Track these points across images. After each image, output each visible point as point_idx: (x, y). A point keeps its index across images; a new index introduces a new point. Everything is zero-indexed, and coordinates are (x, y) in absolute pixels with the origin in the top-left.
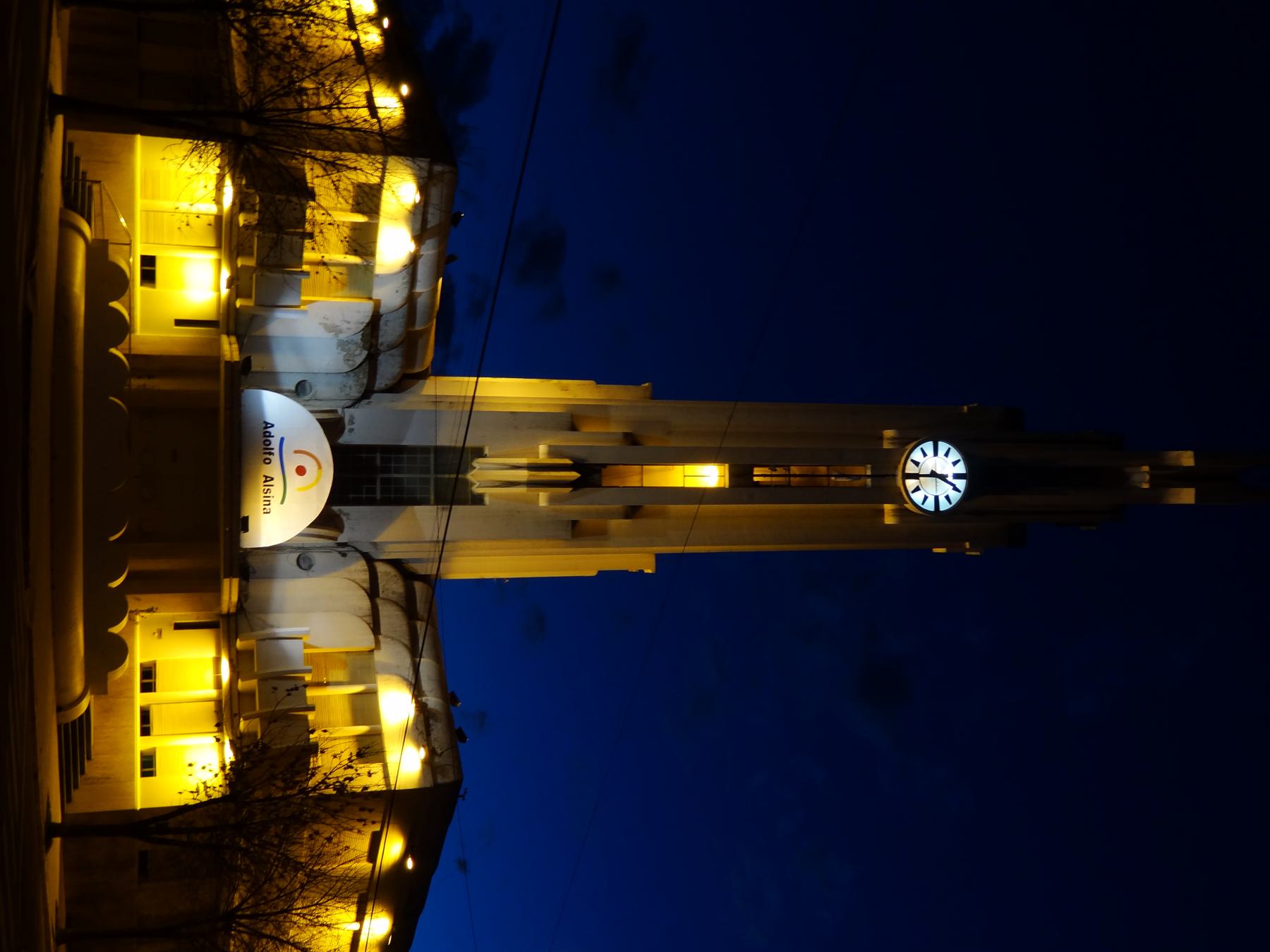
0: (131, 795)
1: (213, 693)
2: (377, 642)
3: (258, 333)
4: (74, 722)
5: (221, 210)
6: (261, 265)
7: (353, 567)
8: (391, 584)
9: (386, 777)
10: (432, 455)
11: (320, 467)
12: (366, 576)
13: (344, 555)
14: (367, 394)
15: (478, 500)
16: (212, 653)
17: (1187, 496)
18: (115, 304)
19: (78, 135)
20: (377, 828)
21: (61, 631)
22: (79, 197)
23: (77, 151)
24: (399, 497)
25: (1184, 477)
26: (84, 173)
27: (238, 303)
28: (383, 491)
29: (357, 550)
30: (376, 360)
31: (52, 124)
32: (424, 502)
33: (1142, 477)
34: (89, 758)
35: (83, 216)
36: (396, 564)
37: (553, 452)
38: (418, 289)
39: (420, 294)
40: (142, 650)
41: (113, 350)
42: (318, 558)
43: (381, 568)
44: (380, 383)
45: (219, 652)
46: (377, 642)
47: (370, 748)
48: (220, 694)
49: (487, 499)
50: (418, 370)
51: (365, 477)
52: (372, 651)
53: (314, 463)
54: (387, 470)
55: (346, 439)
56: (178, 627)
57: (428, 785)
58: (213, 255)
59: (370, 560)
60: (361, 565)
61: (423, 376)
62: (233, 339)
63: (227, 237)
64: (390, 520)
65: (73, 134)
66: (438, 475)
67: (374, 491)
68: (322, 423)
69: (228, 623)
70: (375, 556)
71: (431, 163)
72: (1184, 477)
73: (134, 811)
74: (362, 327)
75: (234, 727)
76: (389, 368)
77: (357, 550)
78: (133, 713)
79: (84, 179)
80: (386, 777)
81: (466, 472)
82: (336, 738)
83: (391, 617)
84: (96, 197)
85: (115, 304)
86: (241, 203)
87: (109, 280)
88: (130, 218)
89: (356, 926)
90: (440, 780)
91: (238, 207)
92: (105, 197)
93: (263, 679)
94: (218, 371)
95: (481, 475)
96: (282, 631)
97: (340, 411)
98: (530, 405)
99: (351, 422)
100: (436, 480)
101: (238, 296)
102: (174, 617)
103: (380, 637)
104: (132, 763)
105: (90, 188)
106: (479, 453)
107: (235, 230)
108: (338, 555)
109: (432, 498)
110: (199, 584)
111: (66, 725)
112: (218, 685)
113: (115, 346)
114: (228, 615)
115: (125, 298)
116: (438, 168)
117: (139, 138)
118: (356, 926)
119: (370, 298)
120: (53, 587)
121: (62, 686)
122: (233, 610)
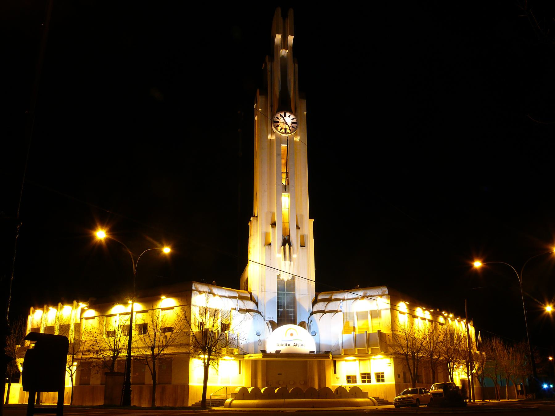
0: (391, 385)
1: (357, 362)
2: (341, 311)
7: (316, 318)
8: (320, 306)
9: (386, 309)
13: (311, 321)
17: (291, 38)
21: (357, 404)
22: (220, 402)
24: (293, 303)
25: (284, 38)
27: (236, 353)
32: (294, 295)
33: (284, 52)
37: (279, 252)
40: (343, 383)
43: (315, 309)
46: (341, 311)
47: (375, 314)
50: (250, 296)
51: (286, 315)
54: (284, 307)
56: (335, 372)
59: (312, 313)
64: (300, 305)
66: (286, 290)
67: (291, 311)
71: (435, 315)
72: (284, 38)
75: (369, 356)
76: (251, 305)
80: (386, 309)
81: (284, 281)
83: (332, 306)
89: (419, 318)
90: (387, 293)
94: (267, 361)
95: (286, 278)
96: (340, 342)
104: (380, 385)
112: (355, 360)
116: (194, 288)
118: (427, 320)
121: (367, 404)
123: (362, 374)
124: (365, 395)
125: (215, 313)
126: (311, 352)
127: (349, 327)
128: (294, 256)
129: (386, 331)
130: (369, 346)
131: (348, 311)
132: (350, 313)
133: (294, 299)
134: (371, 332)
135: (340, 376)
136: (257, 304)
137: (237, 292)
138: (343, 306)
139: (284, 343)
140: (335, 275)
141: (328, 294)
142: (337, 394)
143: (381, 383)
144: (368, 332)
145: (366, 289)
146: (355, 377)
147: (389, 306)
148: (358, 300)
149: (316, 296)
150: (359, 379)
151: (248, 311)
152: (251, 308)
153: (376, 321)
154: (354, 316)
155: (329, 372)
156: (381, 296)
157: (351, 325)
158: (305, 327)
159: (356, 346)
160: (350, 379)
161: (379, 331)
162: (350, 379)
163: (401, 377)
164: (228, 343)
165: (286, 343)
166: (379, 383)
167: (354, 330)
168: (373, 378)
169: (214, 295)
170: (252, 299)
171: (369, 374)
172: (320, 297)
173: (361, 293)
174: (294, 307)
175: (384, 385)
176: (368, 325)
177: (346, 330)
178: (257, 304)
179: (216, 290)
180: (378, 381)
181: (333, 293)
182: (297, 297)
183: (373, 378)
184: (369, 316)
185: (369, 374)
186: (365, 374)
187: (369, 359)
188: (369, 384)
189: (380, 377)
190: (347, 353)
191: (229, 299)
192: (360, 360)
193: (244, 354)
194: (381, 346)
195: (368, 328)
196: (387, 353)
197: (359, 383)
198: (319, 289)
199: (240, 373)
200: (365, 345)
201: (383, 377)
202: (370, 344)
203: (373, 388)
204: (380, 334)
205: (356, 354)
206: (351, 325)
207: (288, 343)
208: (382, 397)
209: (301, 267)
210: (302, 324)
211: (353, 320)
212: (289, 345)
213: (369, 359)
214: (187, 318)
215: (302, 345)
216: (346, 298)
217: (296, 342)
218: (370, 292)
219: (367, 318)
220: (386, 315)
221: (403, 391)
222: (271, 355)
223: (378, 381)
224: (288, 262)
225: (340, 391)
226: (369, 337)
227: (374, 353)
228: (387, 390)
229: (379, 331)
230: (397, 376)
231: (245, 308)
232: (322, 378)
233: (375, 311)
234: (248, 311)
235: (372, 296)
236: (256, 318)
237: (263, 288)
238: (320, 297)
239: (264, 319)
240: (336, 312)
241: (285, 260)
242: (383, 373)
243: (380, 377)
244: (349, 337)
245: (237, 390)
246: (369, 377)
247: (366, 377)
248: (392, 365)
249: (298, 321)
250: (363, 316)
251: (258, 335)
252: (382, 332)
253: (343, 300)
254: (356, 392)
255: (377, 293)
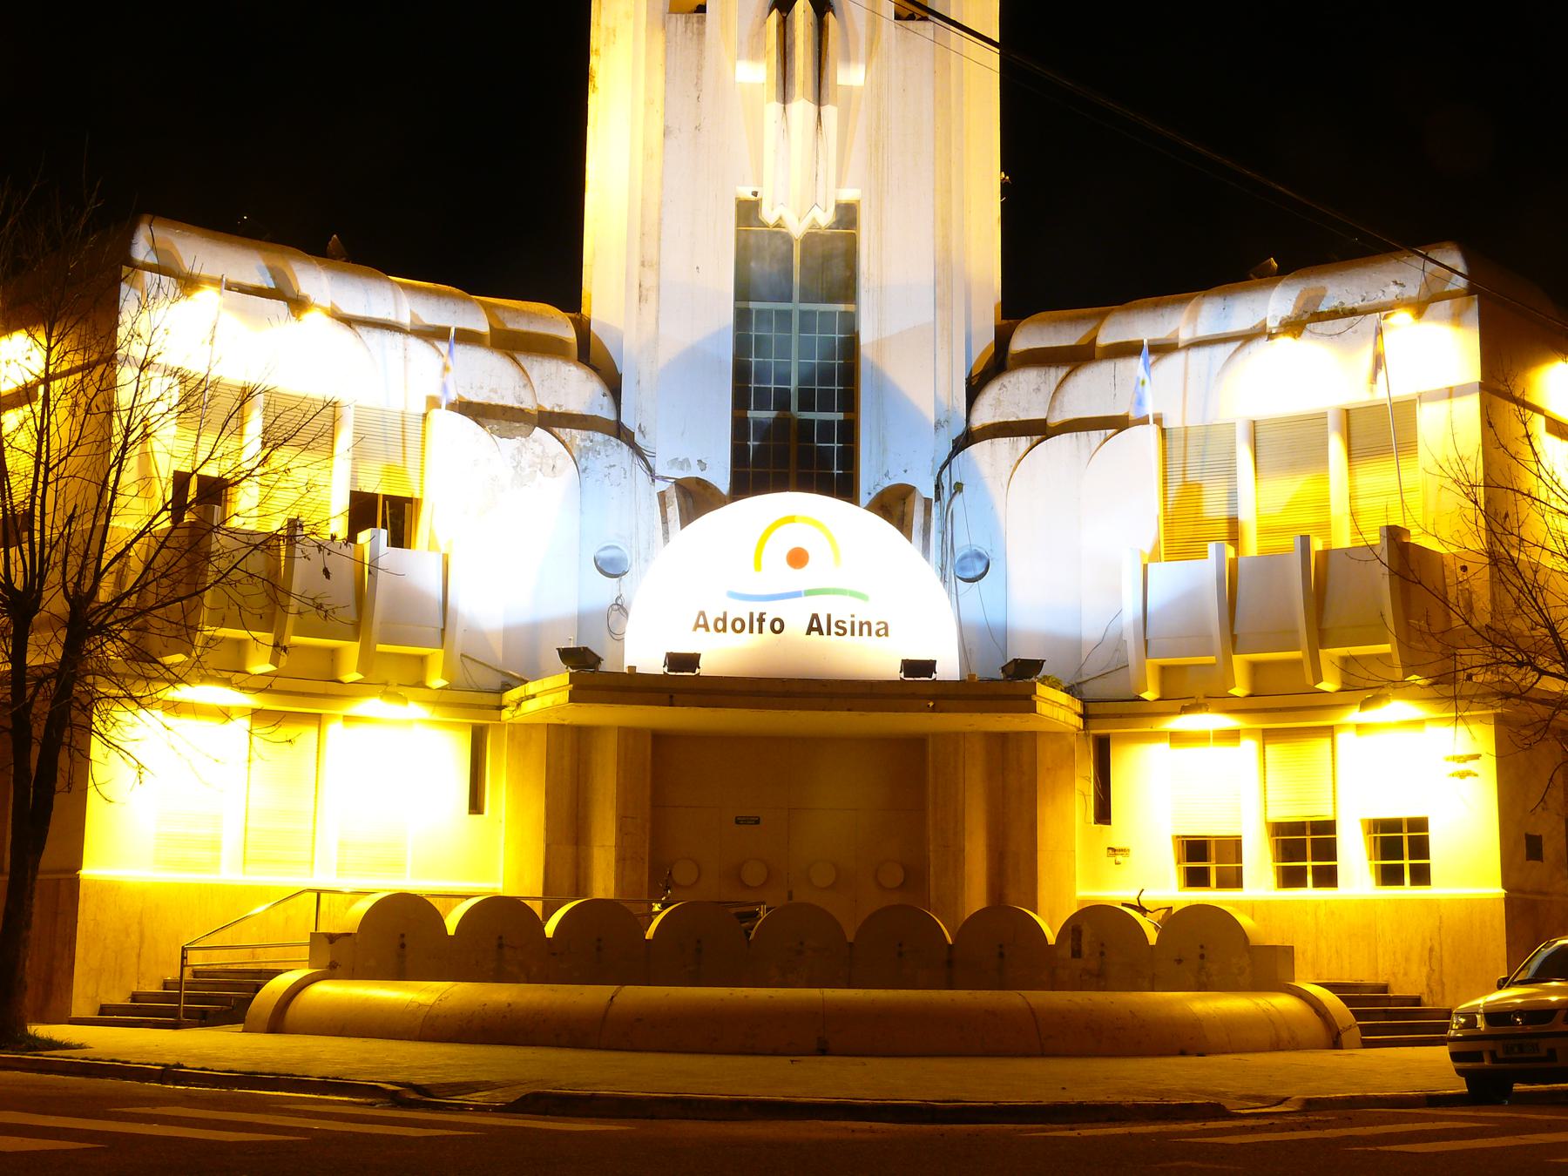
0: (1472, 905)
1: (1250, 745)
2: (1144, 421)
3: (500, 655)
4: (1357, 1015)
5: (242, 711)
6: (357, 628)
9: (1451, 393)
10: (753, 305)
11: (790, 519)
12: (1003, 443)
13: (959, 487)
14: (619, 432)
15: (847, 215)
16: (1161, 748)
18: (451, 924)
19: (85, 994)
20: (1538, 424)
21: (1189, 1040)
22: (220, 996)
23: (119, 998)
24: (842, 376)
26: (166, 985)
28: (827, 408)
29: (948, 462)
30: (552, 414)
31: (52, 1045)
34: (1385, 988)
35: (258, 988)
36: (975, 388)
37: (755, 54)
38: (405, 320)
39: (413, 315)
40: (1148, 882)
41: (550, 929)
42: (962, 543)
43: (985, 414)
44: (605, 411)
45: (1158, 736)
47: (1377, 433)
48: (1250, 732)
49: (848, 195)
52: (1163, 431)
53: (768, 545)
54: (782, 401)
55: (721, 479)
56: (1103, 814)
57: (1473, 315)
58: (333, 728)
59: (967, 439)
60: (977, 451)
61: (583, 329)
62: (512, 695)
63: (302, 693)
64: (879, 376)
65: (81, 1004)
67: (826, 426)
68: (687, 517)
69: (1097, 716)
70: (959, 429)
73: (1509, 901)
74: (659, 38)
75: (1327, 704)
76: (574, 389)
77: (948, 462)
78: (1285, 904)
79: (179, 984)
80: (1451, 393)
81: (788, 240)
82: (1349, 506)
83: (1090, 391)
84: (219, 959)
85: (451, 924)
86: (232, 671)
87: (399, 934)
88: (259, 894)
91: (238, 677)
92: (216, 940)
93: (1234, 642)
94: (660, 739)
95: (798, 211)
96: (1130, 610)
97: (661, 486)
98: (649, 102)
99: (685, 463)
100: (805, 298)
101: (421, 684)
102: (1086, 822)
103: (1133, 415)
104: (1399, 904)
105: (195, 974)
106: (748, 211)
107: (278, 684)
108: (958, 497)
109: (842, 307)
110: (1015, 779)
111: (1365, 1030)
112: (1233, 735)
113: (541, 927)
114: (1085, 716)
115: (438, 904)
116: (141, 250)
117: (86, 873)
119: (425, 415)
120: (1183, 1053)
121: (1278, 1037)
122: (1078, 707)
123: (1279, 829)
124: (1267, 966)
125: (300, 428)
126: (911, 667)
127: (1199, 521)
128: (849, 76)
129: (1445, 526)
130: (1321, 637)
131: (1193, 421)
132: (1207, 432)
133: (851, 346)
134: (1343, 539)
135: (1136, 833)
136: (613, 385)
137: (482, 303)
138: (1158, 388)
139: (742, 610)
140: (1121, 207)
141: (1074, 320)
142: (1077, 953)
143: (1407, 891)
144: (1317, 545)
145: (1319, 274)
146: (1233, 847)
147: (1474, 374)
148: (1260, 348)
149: (1002, 338)
150: (1260, 862)
151: (550, 420)
152: (575, 406)
153: (1378, 478)
154: (1232, 453)
155: (1065, 813)
156: (1420, 307)
157: (1214, 506)
158: (903, 525)
159: (1234, 642)
160: (1201, 857)
161: (1394, 534)
162: (1201, 857)
163: (1548, 850)
164: (355, 609)
165: (757, 608)
166: (1393, 892)
167: (1234, 536)
168: (1355, 856)
169: (298, 304)
170: (587, 351)
171: (1329, 827)
172: (1022, 341)
173: (1278, 302)
174: (850, 402)
175: (1427, 904)
176: (1323, 505)
177: (1180, 542)
178: (613, 385)
179: (313, 281)
180: (1390, 876)
181: (1102, 317)
182: (867, 336)
183: (1355, 856)
184: (1336, 446)
185: (1329, 827)
186: (1299, 827)
187: (1329, 731)
188: (1325, 893)
189: (1402, 848)
190: (1186, 690)
191: (416, 344)
192: (1268, 736)
193: (506, 687)
194: (1404, 644)
195: (1324, 528)
196: (1448, 685)
197: (1256, 895)
198: (1021, 298)
199: (476, 806)
200: (1306, 630)
201: (1420, 848)
202: (1328, 624)
203: (1348, 922)
204: (1400, 550)
205: (1240, 690)
206: (1214, 506)
207: (772, 611)
208: (1409, 982)
209: (910, 166)
210: (894, 506)
211: (1230, 472)
212: (778, 627)
213: (1329, 731)
214: (103, 441)
215: (864, 627)
216: (1185, 336)
217: (839, 609)
218: (1339, 289)
219: (1316, 458)
220: (1452, 431)
221: (1544, 951)
222: (633, 687)
223: (1390, 876)
224: (802, 106)
225: (1101, 929)
226: (1323, 578)
227: (1363, 685)
228: (1447, 938)
229: (1394, 534)
230: (1523, 848)
231: (529, 404)
232: (1015, 858)
233: (1375, 411)
234: (550, 420)
235: (1353, 312)
236: (597, 464)
237: (650, 281)
238: (1022, 341)
239: (650, 470)
240: (1118, 424)
241: (785, 96)
242: (1420, 825)
243: (1402, 848)
244: (1189, 581)
245: (349, 916)
246: (1327, 850)
247: (1306, 849)
248: (1488, 769)
249: (870, 480)
250: (1289, 445)
251: (610, 568)
252: (1417, 538)
253: (1162, 349)
254: (1207, 947)
255: (1393, 292)
